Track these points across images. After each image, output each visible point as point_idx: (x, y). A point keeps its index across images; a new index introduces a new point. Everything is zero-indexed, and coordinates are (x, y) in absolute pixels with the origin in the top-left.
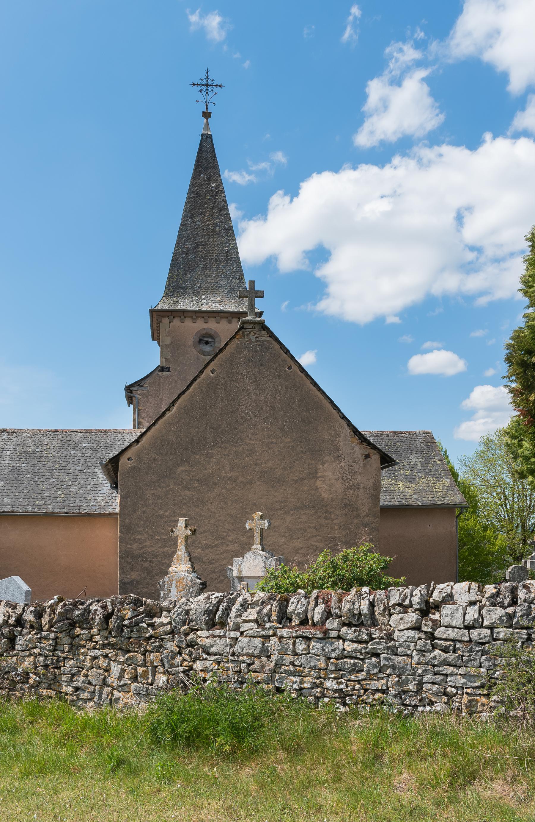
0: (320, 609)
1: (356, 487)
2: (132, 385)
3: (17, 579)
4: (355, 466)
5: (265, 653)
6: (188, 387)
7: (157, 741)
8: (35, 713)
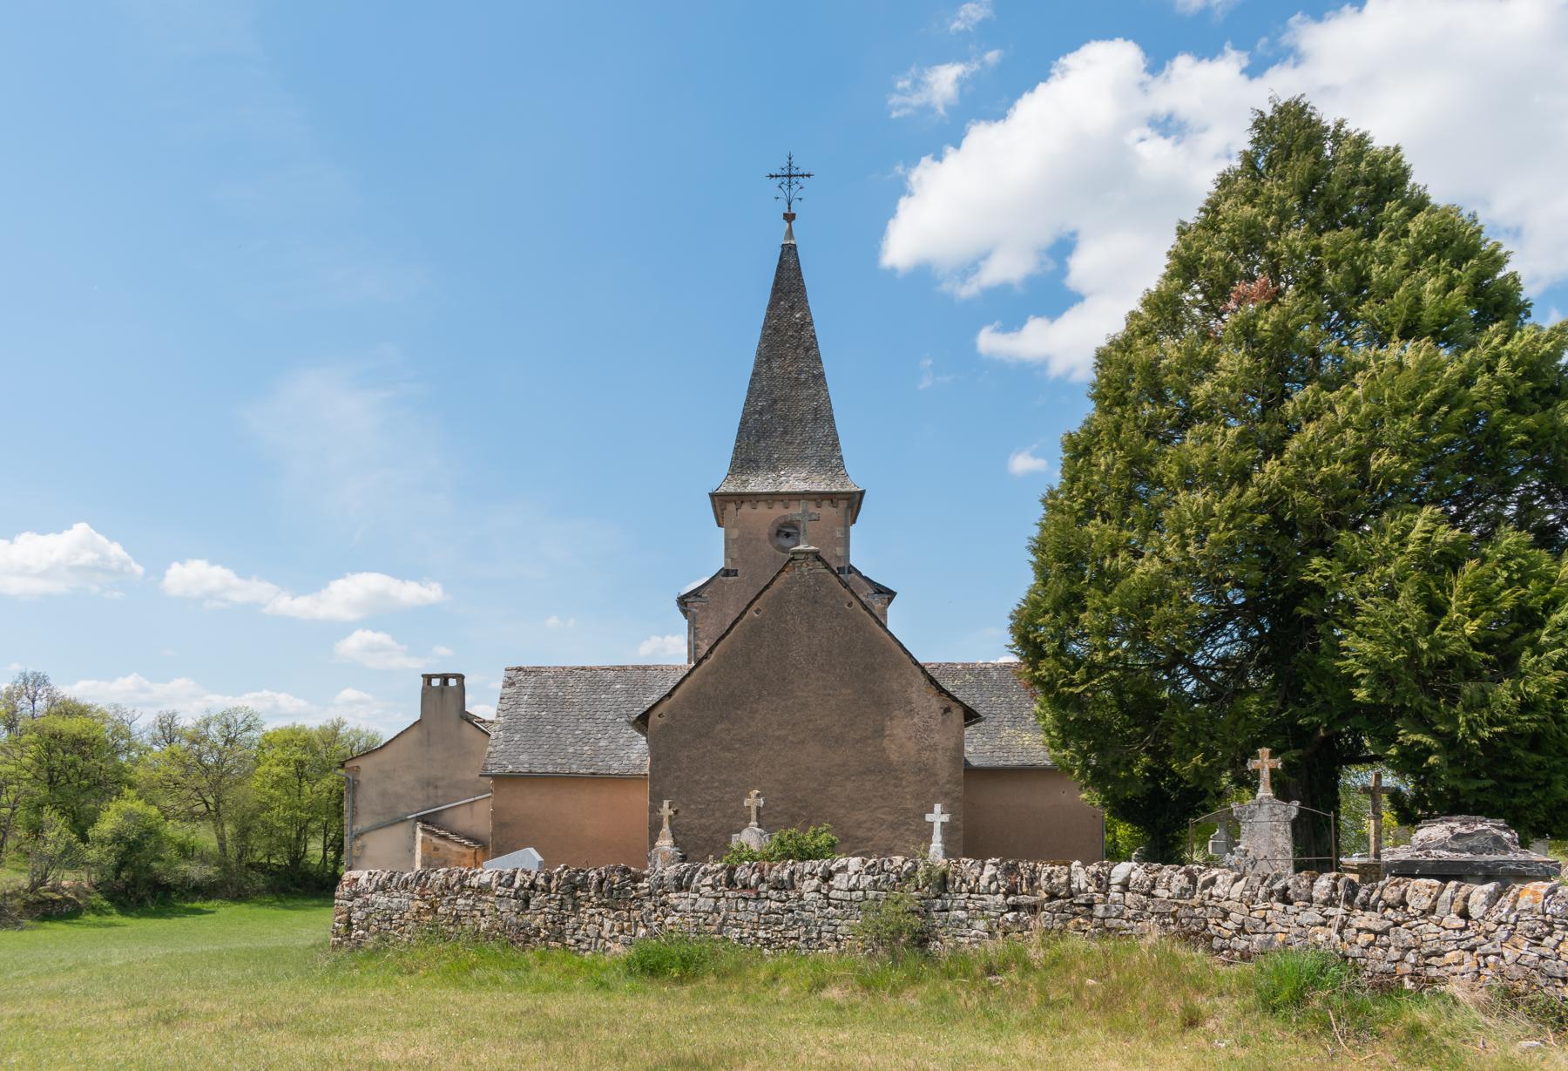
0: (755, 877)
1: (933, 748)
2: (687, 596)
3: (532, 850)
4: (932, 723)
5: (716, 910)
6: (728, 631)
7: (631, 973)
8: (543, 959)
